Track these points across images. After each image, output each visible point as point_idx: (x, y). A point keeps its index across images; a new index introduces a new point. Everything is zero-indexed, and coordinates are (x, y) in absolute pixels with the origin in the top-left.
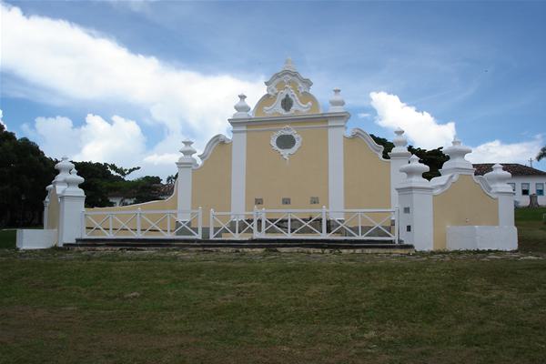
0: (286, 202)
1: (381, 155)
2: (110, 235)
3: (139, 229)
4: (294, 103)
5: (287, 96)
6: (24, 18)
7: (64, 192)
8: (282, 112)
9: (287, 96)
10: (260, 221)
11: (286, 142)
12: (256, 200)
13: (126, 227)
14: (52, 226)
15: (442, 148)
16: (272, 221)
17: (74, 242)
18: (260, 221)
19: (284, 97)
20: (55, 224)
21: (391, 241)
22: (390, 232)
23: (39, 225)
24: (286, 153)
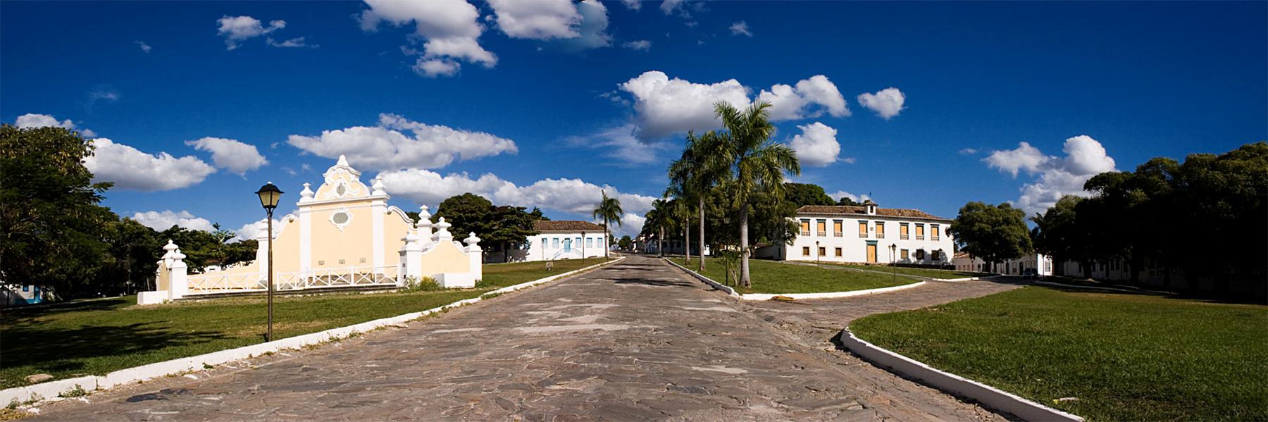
0: (342, 262)
1: (412, 227)
2: (206, 292)
3: (226, 288)
4: (347, 189)
5: (341, 184)
6: (475, 19)
7: (171, 265)
8: (338, 196)
9: (341, 184)
10: (968, 266)
11: (341, 218)
12: (319, 262)
13: (198, 287)
14: (164, 288)
15: (525, 208)
16: (318, 277)
17: (182, 298)
18: (968, 266)
19: (338, 185)
20: (166, 287)
21: (395, 285)
22: (347, 279)
23: (154, 288)
24: (341, 226)
